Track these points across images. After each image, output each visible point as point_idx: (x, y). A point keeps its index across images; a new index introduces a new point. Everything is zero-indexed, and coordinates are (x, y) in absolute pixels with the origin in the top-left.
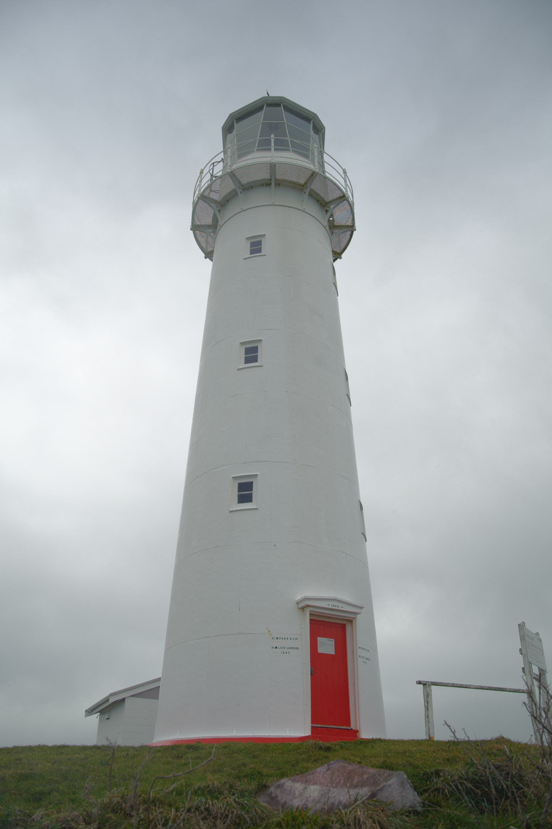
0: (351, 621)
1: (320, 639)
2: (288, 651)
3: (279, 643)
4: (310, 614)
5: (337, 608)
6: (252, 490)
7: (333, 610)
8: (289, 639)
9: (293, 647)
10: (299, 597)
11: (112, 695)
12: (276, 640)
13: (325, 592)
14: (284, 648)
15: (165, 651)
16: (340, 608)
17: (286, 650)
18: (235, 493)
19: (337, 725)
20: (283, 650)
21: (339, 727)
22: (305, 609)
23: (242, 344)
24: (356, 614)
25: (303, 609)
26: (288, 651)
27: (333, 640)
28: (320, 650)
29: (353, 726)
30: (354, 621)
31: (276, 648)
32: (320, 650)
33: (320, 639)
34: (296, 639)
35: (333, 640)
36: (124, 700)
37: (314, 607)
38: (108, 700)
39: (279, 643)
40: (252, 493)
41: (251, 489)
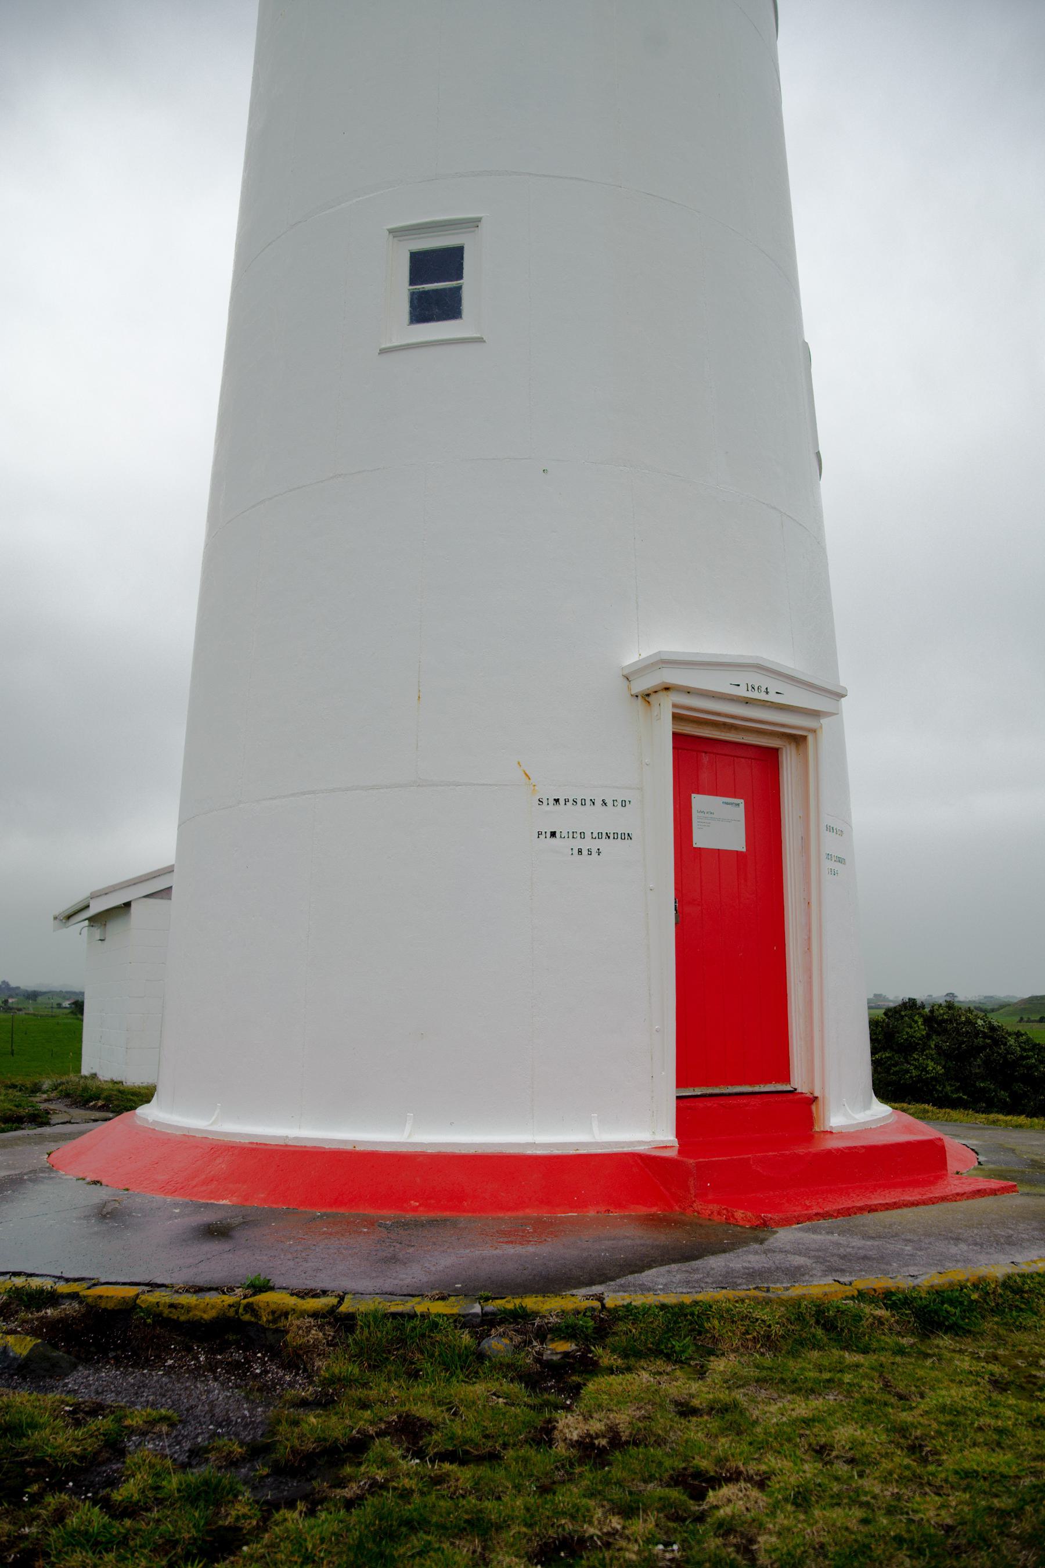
0: (798, 740)
1: (699, 802)
2: (594, 845)
3: (562, 819)
4: (676, 717)
5: (762, 696)
6: (459, 274)
7: (747, 702)
8: (599, 802)
9: (611, 831)
10: (631, 658)
11: (95, 896)
12: (552, 807)
13: (717, 643)
14: (582, 835)
15: (179, 826)
16: (772, 697)
17: (586, 844)
18: (399, 289)
19: (751, 1083)
20: (578, 843)
21: (757, 1088)
22: (653, 699)
23: (397, 233)
24: (816, 714)
25: (646, 696)
26: (594, 845)
27: (741, 802)
28: (701, 839)
29: (799, 1081)
30: (810, 739)
31: (553, 834)
32: (701, 839)
33: (699, 802)
34: (624, 804)
35: (741, 802)
36: (128, 905)
37: (688, 691)
38: (88, 906)
39: (562, 819)
40: (459, 289)
41: (458, 273)
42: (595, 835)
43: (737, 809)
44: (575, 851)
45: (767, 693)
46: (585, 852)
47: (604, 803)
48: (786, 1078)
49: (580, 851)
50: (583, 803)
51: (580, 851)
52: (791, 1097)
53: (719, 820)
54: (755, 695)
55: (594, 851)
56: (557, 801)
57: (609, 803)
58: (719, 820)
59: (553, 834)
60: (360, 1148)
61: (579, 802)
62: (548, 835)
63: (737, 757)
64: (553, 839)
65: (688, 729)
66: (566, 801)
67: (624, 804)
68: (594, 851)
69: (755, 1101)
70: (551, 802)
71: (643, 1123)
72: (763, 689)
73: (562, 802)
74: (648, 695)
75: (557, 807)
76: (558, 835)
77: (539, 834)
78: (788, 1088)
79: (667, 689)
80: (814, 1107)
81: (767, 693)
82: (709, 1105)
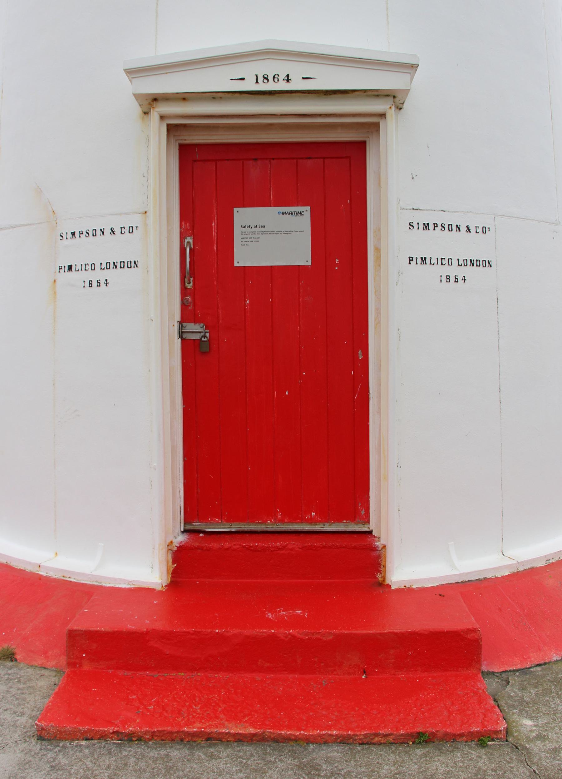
5: (282, 86)
8: (108, 231)
9: (118, 260)
16: (297, 85)
17: (453, 271)
20: (446, 270)
28: (245, 255)
32: (245, 255)
34: (131, 230)
42: (104, 266)
43: (299, 218)
47: (468, 230)
49: (91, 284)
50: (426, 226)
53: (272, 233)
54: (271, 86)
55: (103, 282)
56: (73, 234)
58: (272, 233)
59: (70, 268)
60: (14, 564)
62: (67, 269)
64: (70, 273)
65: (215, 137)
66: (81, 233)
67: (131, 230)
68: (103, 282)
69: (294, 544)
72: (282, 76)
75: (74, 240)
77: (411, 259)
78: (367, 529)
81: (288, 81)
82: (227, 545)
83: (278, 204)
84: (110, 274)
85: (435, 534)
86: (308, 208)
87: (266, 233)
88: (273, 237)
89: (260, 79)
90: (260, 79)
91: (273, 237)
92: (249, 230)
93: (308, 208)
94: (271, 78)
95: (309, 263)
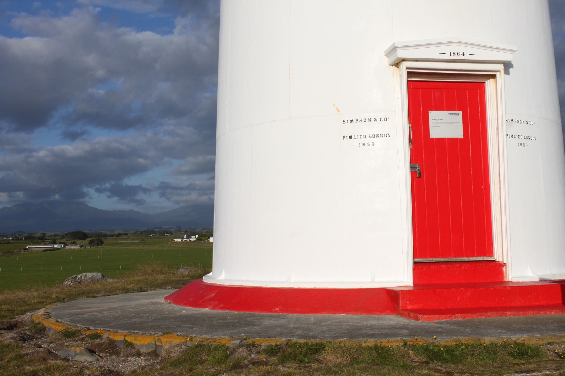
3: (351, 129)
5: (461, 57)
8: (373, 120)
12: (350, 124)
16: (467, 57)
17: (365, 141)
20: (363, 140)
21: (472, 259)
28: (435, 133)
29: (498, 256)
31: (350, 137)
32: (435, 133)
39: (351, 129)
42: (371, 136)
43: (457, 116)
44: (361, 145)
45: (463, 55)
46: (366, 144)
47: (376, 120)
48: (491, 253)
49: (364, 145)
51: (364, 145)
52: (493, 263)
53: (446, 123)
54: (453, 57)
55: (371, 143)
56: (352, 121)
57: (378, 119)
58: (446, 123)
61: (363, 121)
62: (348, 137)
63: (494, 76)
67: (386, 119)
68: (371, 143)
70: (349, 121)
71: (395, 270)
72: (461, 53)
73: (354, 121)
74: (398, 64)
76: (353, 137)
77: (344, 137)
78: (492, 259)
79: (8, 252)
80: (504, 269)
81: (463, 55)
83: (447, 110)
84: (374, 140)
85: (523, 252)
86: (461, 112)
87: (443, 123)
88: (446, 125)
89: (452, 54)
90: (452, 54)
91: (446, 125)
92: (436, 121)
93: (461, 112)
94: (456, 54)
95: (431, 137)
